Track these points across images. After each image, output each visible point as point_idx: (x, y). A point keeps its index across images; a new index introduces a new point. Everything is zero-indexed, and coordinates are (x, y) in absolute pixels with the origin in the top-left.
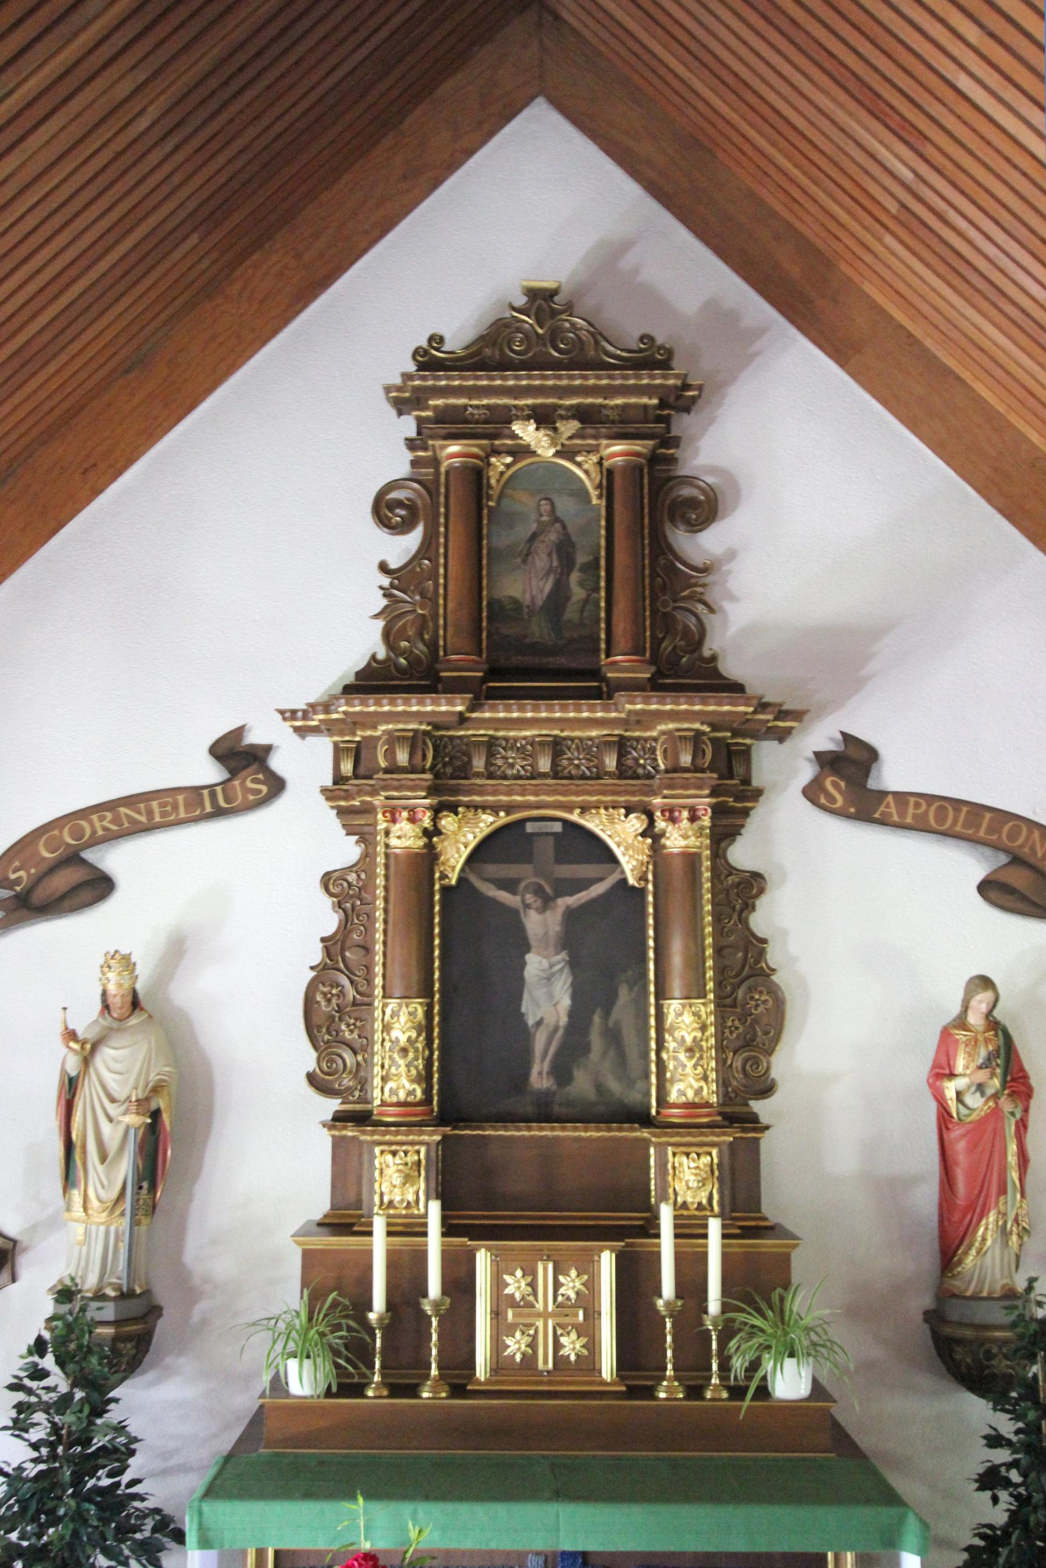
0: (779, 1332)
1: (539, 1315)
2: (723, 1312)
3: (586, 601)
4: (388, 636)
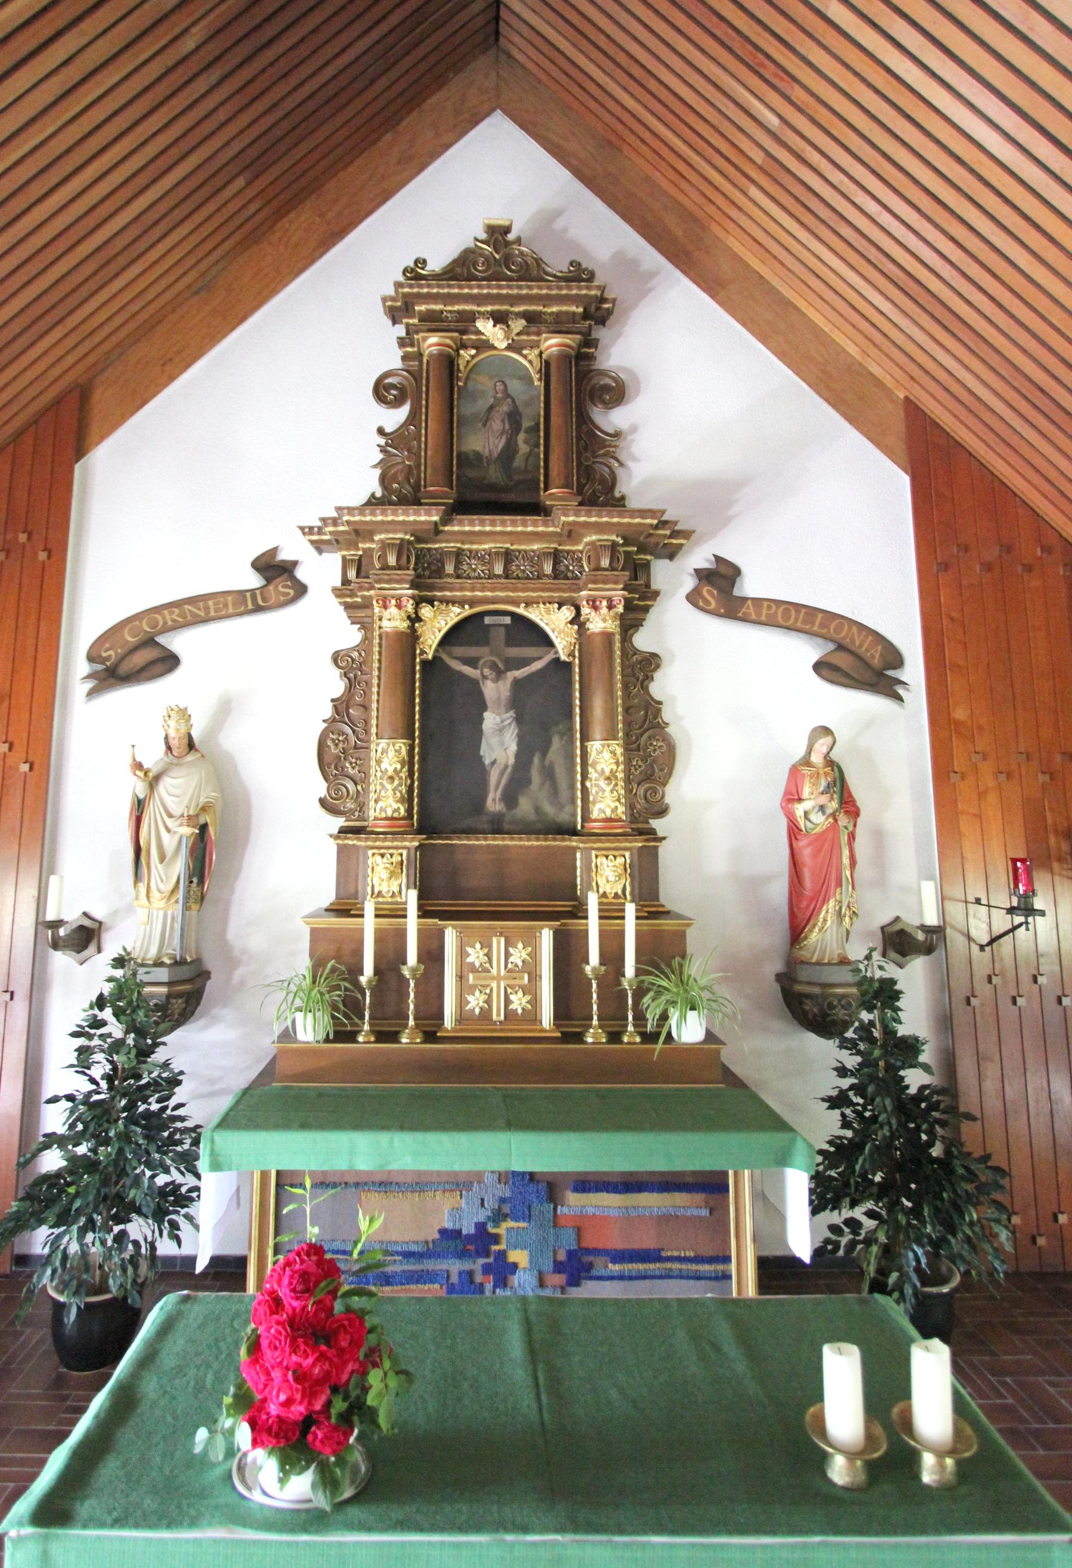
0: (682, 991)
1: (493, 978)
2: (636, 976)
3: (530, 453)
4: (383, 480)
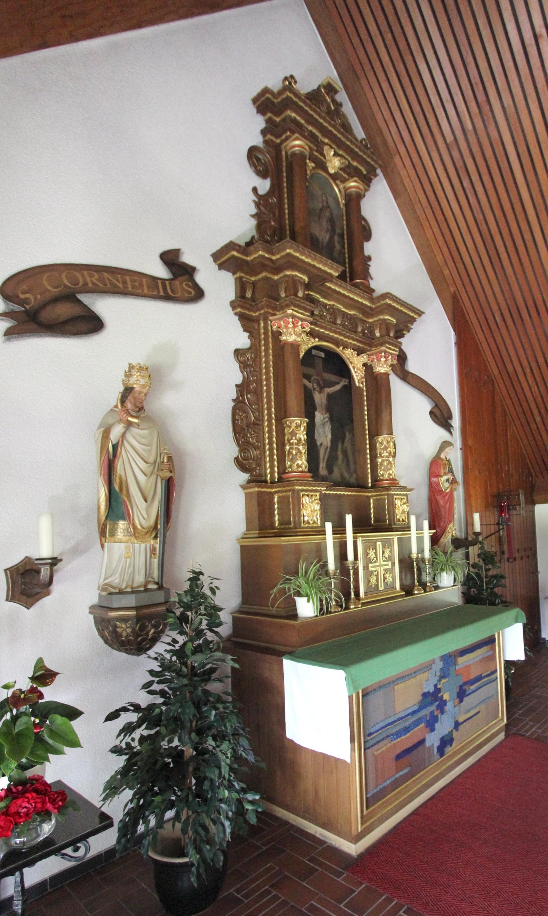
3: (340, 251)
